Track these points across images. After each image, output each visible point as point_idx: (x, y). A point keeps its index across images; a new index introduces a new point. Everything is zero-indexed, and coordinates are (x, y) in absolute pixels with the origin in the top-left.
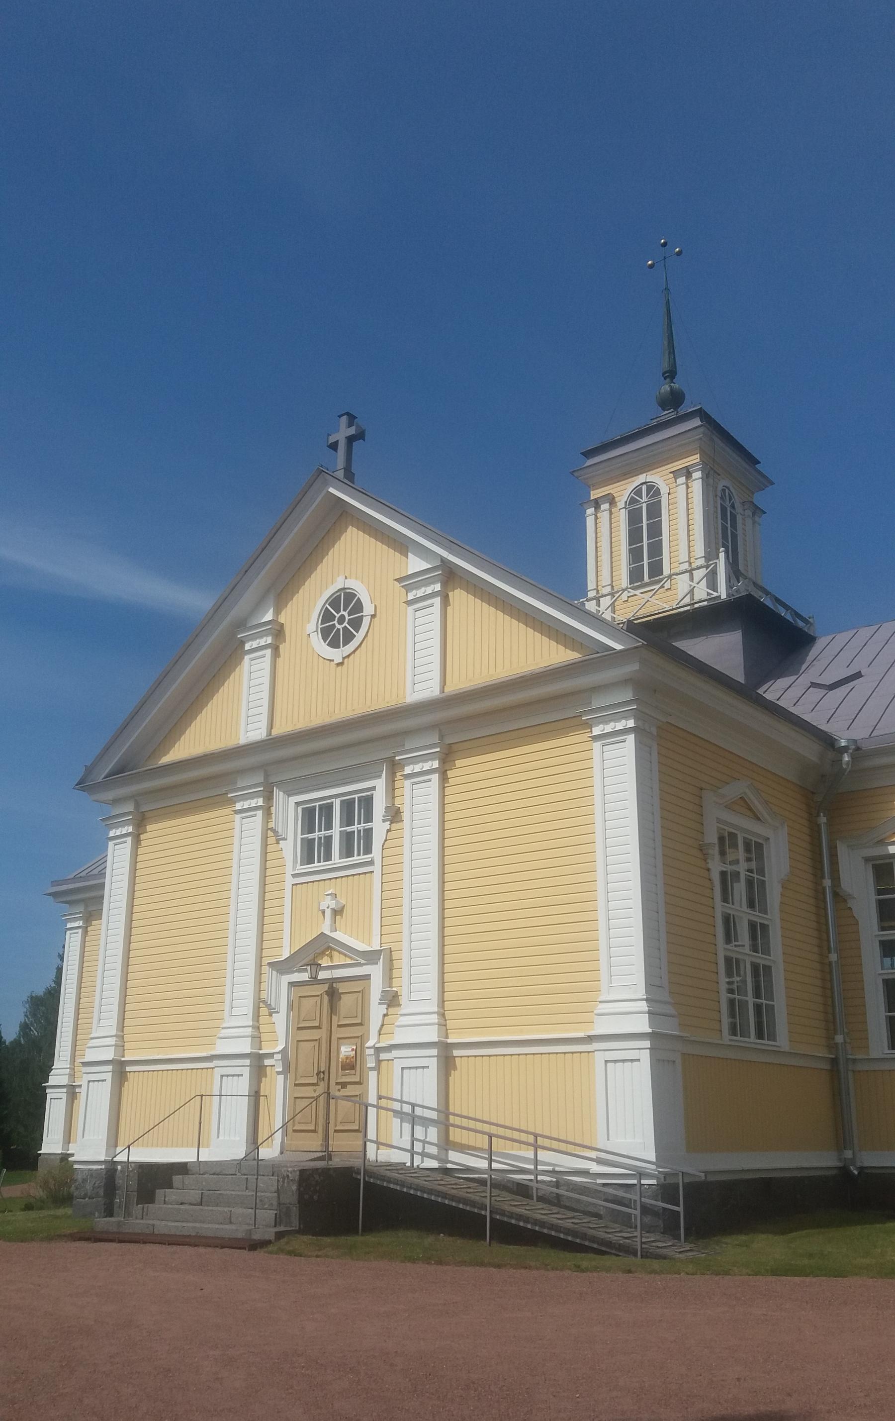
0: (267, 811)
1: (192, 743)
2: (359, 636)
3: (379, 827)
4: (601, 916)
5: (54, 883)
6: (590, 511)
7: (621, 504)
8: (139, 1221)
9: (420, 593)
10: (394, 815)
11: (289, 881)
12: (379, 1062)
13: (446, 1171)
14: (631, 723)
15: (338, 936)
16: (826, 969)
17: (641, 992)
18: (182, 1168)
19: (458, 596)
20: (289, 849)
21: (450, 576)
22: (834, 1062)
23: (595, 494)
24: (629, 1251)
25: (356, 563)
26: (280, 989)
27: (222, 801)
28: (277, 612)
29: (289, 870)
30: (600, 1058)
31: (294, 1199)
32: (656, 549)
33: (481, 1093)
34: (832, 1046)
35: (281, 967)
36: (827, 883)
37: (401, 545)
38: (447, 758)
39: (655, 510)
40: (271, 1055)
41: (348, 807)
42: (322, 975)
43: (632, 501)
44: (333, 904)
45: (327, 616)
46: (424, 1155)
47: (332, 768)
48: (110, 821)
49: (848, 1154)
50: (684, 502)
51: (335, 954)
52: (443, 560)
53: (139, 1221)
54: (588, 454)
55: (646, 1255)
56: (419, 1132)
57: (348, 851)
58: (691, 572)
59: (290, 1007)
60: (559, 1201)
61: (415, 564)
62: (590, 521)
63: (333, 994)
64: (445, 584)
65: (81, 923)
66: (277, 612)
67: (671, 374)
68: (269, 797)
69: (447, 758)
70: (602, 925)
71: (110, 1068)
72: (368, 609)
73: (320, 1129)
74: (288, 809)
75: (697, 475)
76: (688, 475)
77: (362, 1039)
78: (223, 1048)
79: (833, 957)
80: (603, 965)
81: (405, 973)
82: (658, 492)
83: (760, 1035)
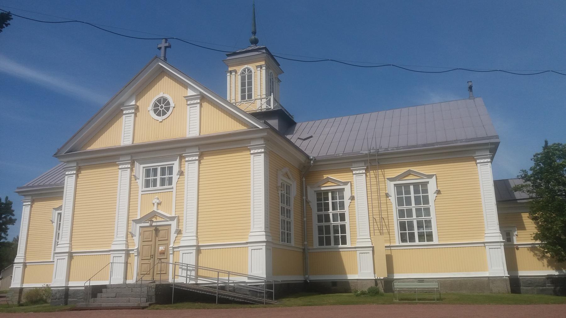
0: (132, 170)
1: (102, 143)
3: (175, 177)
4: (252, 207)
5: (18, 188)
6: (228, 74)
7: (239, 74)
8: (94, 303)
9: (192, 102)
10: (181, 173)
11: (140, 193)
12: (174, 252)
13: (197, 284)
14: (263, 150)
15: (158, 211)
17: (263, 230)
18: (105, 287)
19: (205, 104)
21: (203, 98)
22: (304, 250)
23: (230, 69)
24: (262, 303)
25: (165, 88)
26: (136, 229)
27: (114, 164)
28: (136, 102)
29: (140, 189)
30: (250, 248)
31: (154, 293)
32: (250, 90)
33: (207, 260)
36: (304, 198)
37: (186, 86)
38: (201, 156)
39: (250, 77)
40: (133, 250)
41: (163, 170)
42: (154, 224)
43: (243, 73)
44: (158, 201)
45: (156, 105)
46: (191, 279)
47: (158, 157)
48: (67, 169)
49: (307, 276)
50: (259, 76)
51: (158, 217)
52: (200, 92)
53: (94, 303)
54: (228, 55)
55: (266, 303)
56: (189, 273)
57: (163, 184)
58: (261, 99)
59: (140, 234)
60: (234, 290)
61: (190, 93)
62: (228, 78)
63: (157, 230)
64: (201, 100)
65: (30, 203)
66: (136, 102)
67: (254, 33)
68: (133, 164)
69: (201, 156)
70: (252, 209)
71: (124, 252)
72: (172, 105)
73: (151, 273)
74: (140, 169)
75: (264, 68)
76: (261, 68)
77: (167, 245)
78: (114, 248)
79: (305, 219)
80: (252, 221)
81: (184, 224)
82: (251, 71)
83: (288, 242)
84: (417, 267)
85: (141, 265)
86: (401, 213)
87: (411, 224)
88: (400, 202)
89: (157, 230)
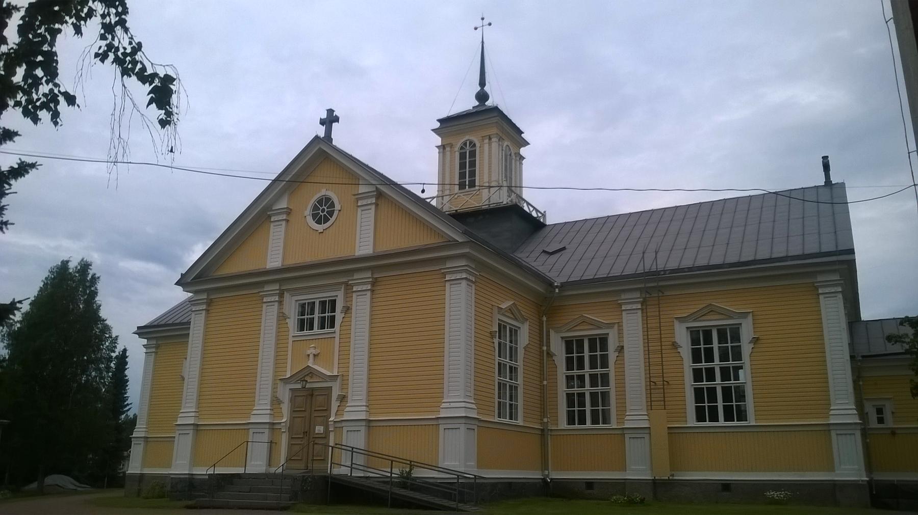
0: (280, 303)
2: (332, 220)
3: (339, 316)
10: (347, 310)
11: (291, 340)
16: (542, 388)
20: (292, 323)
26: (285, 394)
29: (291, 333)
34: (542, 423)
35: (285, 381)
39: (473, 154)
41: (323, 303)
43: (462, 148)
45: (315, 208)
49: (546, 472)
61: (362, 189)
64: (377, 198)
82: (475, 145)
83: (511, 418)
84: (717, 461)
85: (290, 446)
86: (697, 375)
87: (712, 391)
88: (696, 357)
89: (311, 393)
